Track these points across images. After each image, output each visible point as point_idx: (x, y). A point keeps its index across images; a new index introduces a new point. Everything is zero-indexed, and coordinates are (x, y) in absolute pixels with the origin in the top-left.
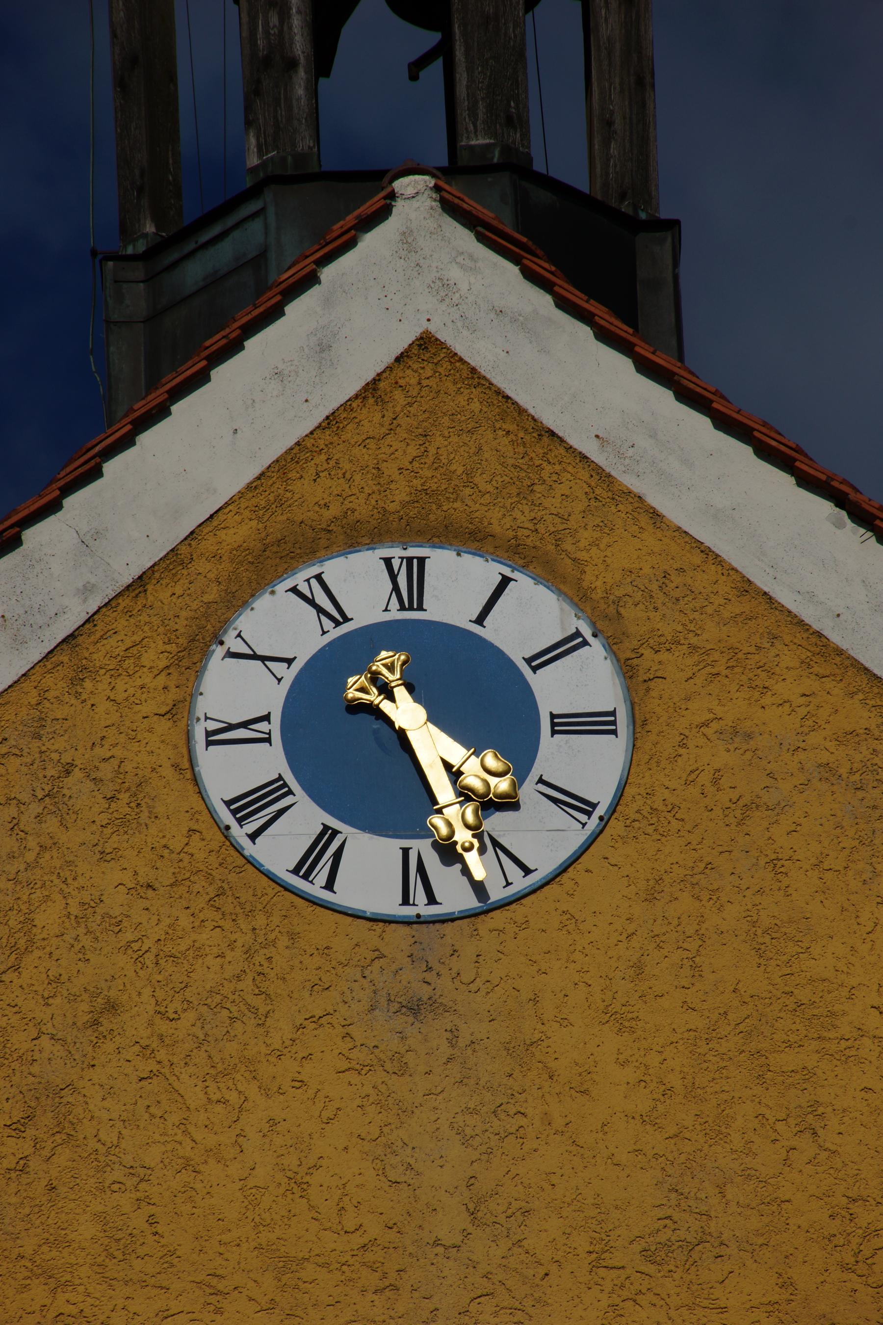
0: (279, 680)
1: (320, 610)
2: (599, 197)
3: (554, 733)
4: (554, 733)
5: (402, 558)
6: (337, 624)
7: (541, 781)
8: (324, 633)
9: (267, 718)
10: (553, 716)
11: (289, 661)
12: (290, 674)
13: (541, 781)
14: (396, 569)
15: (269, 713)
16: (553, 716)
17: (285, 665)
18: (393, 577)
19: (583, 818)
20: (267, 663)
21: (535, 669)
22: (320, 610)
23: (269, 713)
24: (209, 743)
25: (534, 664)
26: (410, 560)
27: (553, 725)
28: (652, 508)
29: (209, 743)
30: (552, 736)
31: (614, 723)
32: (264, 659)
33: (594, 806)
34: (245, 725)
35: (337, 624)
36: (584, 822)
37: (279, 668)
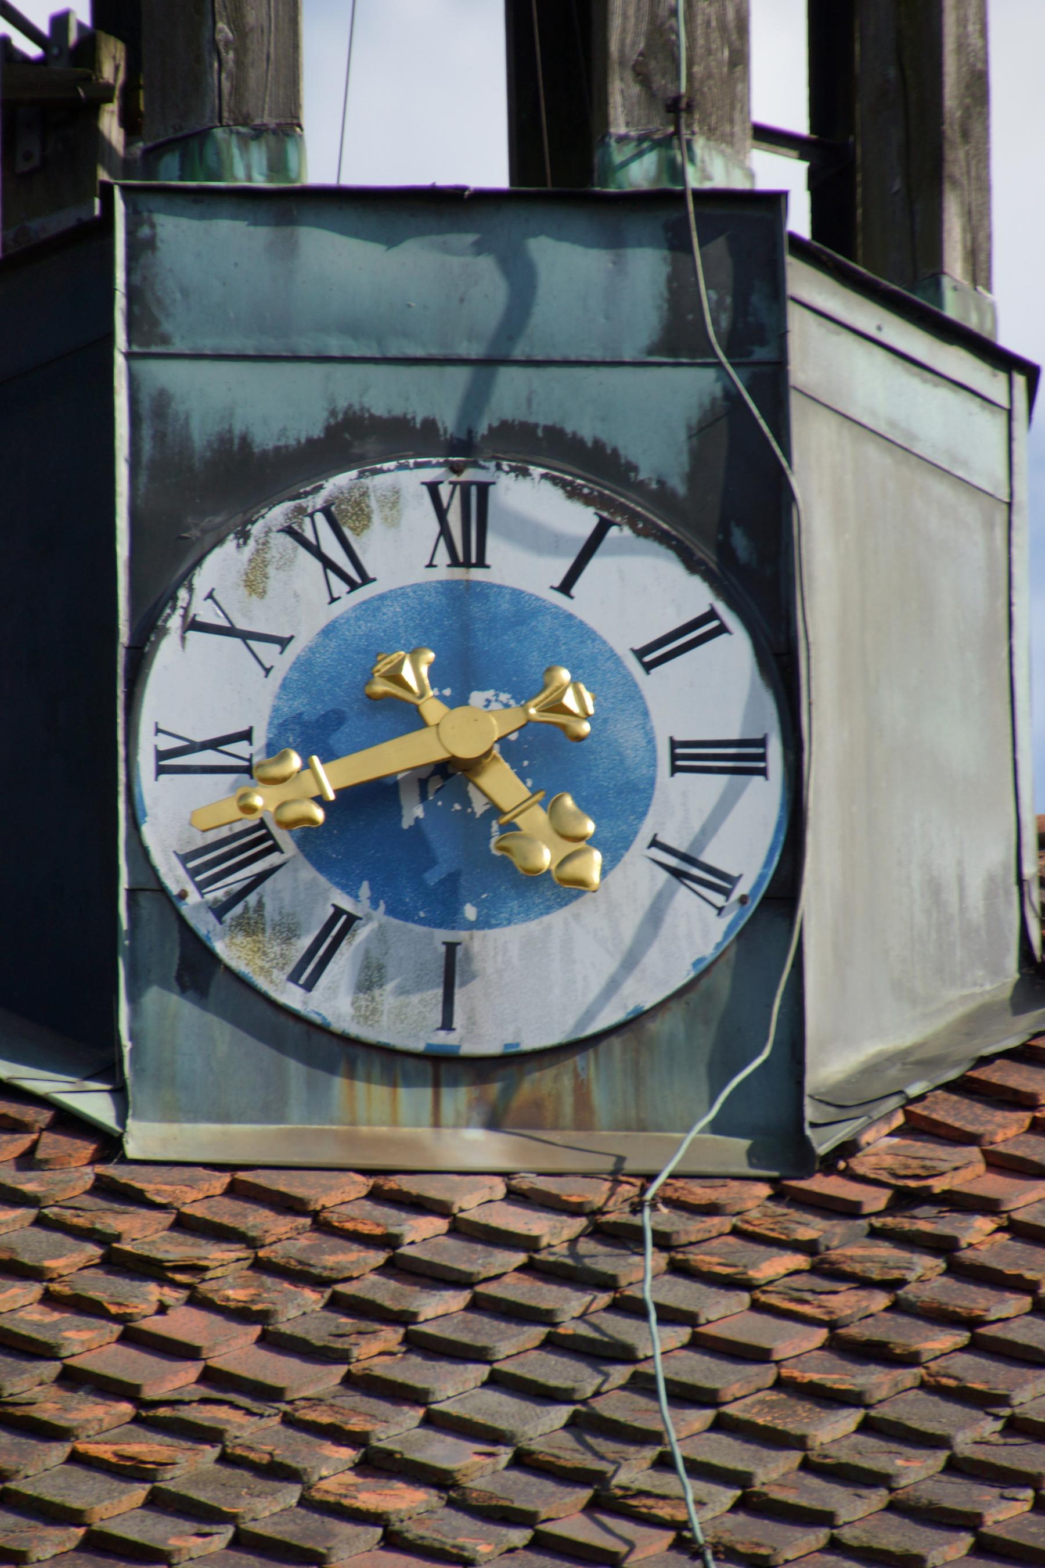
0: (268, 671)
1: (328, 564)
2: (294, 1068)
3: (675, 770)
4: (675, 770)
5: (454, 484)
6: (353, 586)
7: (655, 843)
8: (333, 600)
9: (246, 736)
10: (674, 744)
11: (283, 642)
12: (282, 662)
13: (655, 843)
14: (445, 500)
15: (251, 728)
16: (674, 744)
17: (277, 648)
18: (441, 513)
19: (719, 899)
20: (250, 642)
21: (648, 667)
22: (328, 564)
23: (251, 728)
24: (161, 770)
25: (647, 659)
26: (465, 487)
27: (674, 757)
28: (620, 754)
29: (161, 770)
30: (672, 775)
31: (763, 757)
32: (246, 636)
33: (733, 880)
34: (214, 744)
35: (353, 586)
36: (719, 905)
37: (267, 651)
